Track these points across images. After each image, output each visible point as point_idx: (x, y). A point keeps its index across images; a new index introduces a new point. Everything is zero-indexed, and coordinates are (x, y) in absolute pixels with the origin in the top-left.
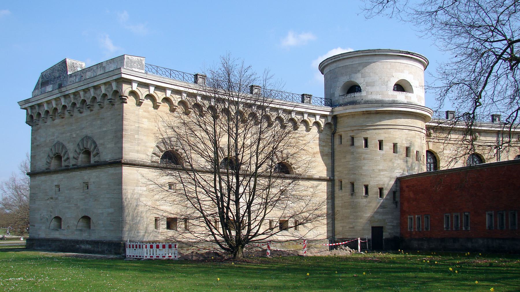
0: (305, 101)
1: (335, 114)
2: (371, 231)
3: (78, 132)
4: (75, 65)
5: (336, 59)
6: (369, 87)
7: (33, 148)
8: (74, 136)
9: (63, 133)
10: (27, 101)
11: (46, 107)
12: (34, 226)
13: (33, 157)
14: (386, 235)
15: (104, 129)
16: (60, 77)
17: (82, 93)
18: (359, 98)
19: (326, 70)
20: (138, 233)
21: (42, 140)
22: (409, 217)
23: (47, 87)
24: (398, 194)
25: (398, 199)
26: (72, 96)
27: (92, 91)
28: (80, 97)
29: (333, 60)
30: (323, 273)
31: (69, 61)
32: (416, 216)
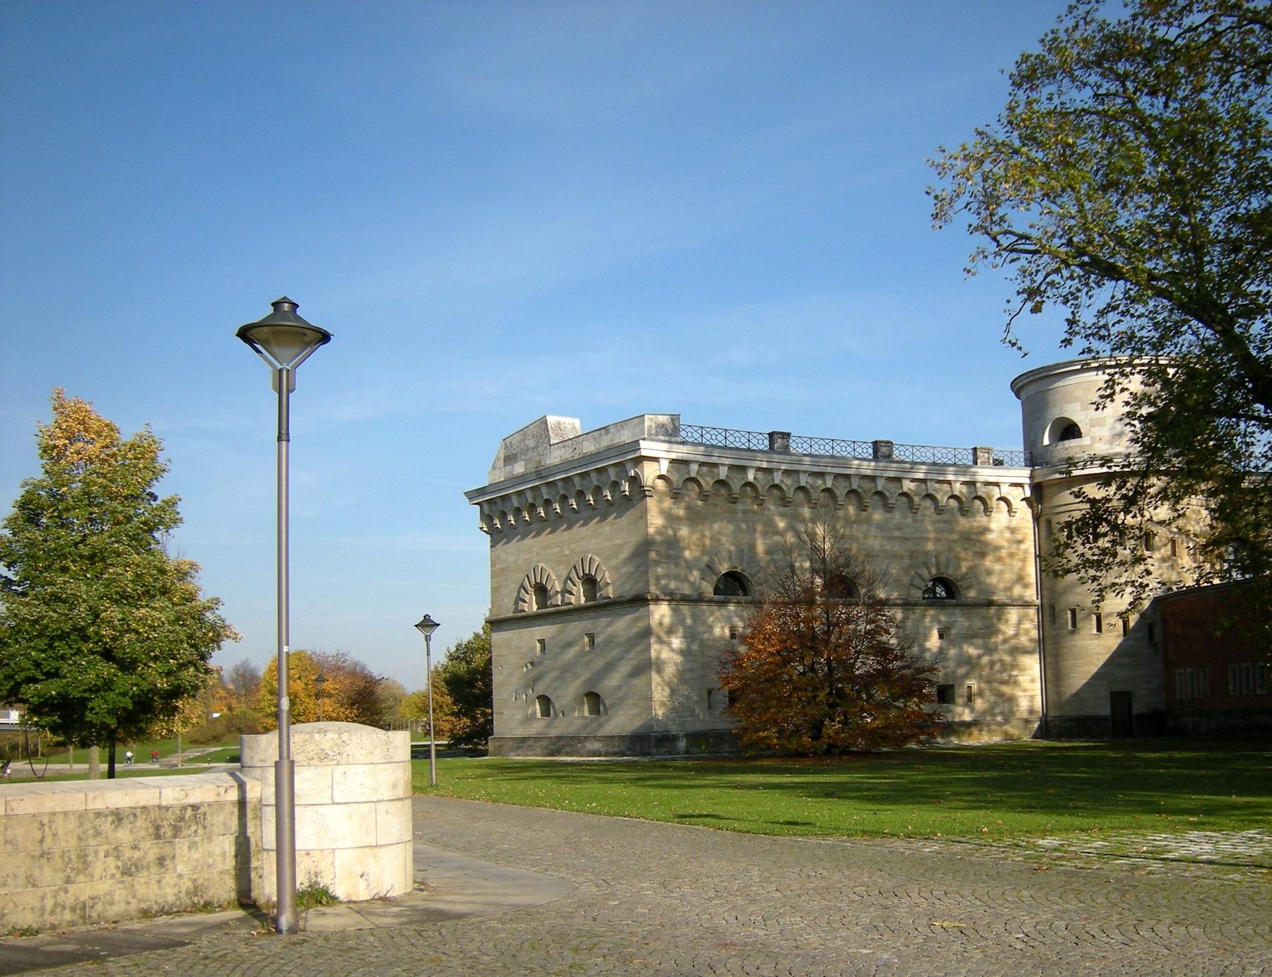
0: (979, 461)
1: (1037, 481)
2: (1109, 701)
3: (573, 546)
4: (562, 426)
5: (1036, 377)
6: (1096, 429)
7: (494, 575)
8: (567, 552)
9: (548, 548)
10: (481, 491)
11: (515, 502)
12: (502, 714)
13: (495, 590)
14: (1138, 708)
15: (618, 542)
16: (537, 447)
17: (576, 480)
18: (1078, 450)
19: (1024, 394)
20: (1237, 455)
21: (511, 559)
22: (1177, 671)
23: (516, 465)
24: (1158, 630)
25: (1158, 638)
26: (560, 484)
27: (594, 476)
28: (574, 485)
29: (1031, 378)
30: (669, 767)
31: (551, 420)
32: (1188, 670)
